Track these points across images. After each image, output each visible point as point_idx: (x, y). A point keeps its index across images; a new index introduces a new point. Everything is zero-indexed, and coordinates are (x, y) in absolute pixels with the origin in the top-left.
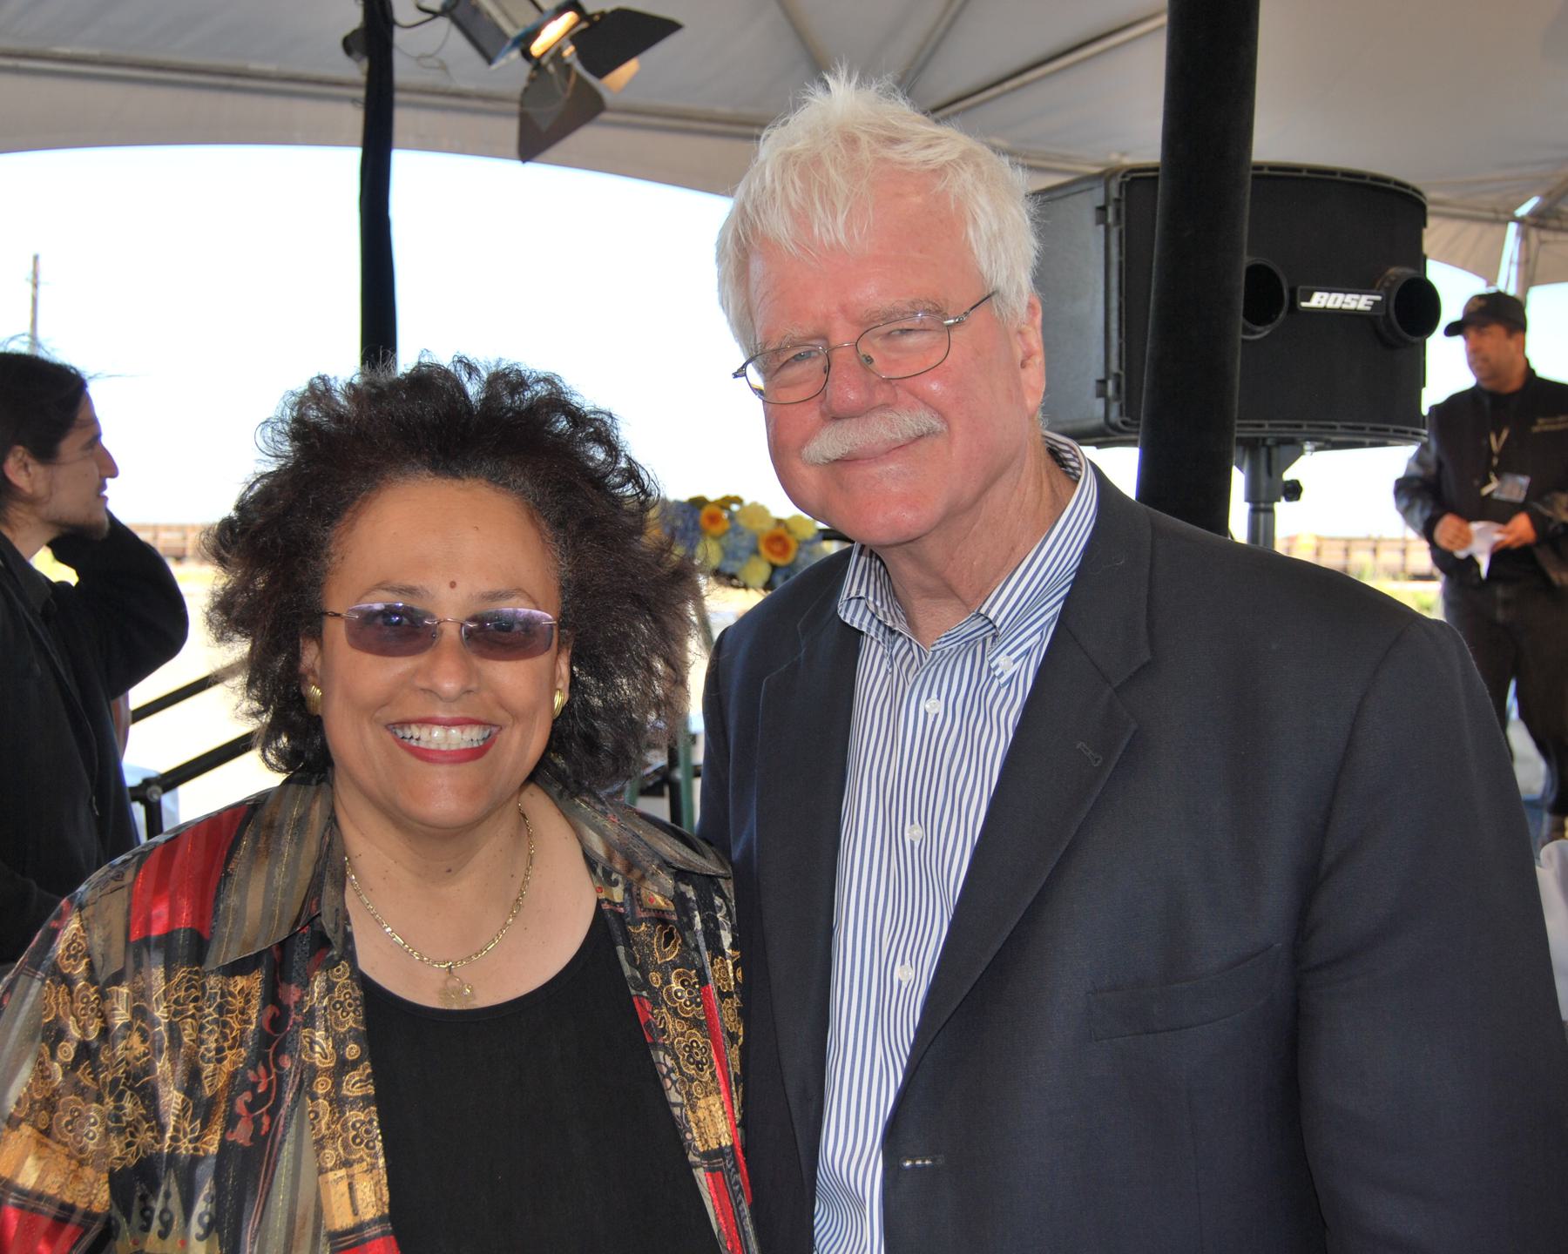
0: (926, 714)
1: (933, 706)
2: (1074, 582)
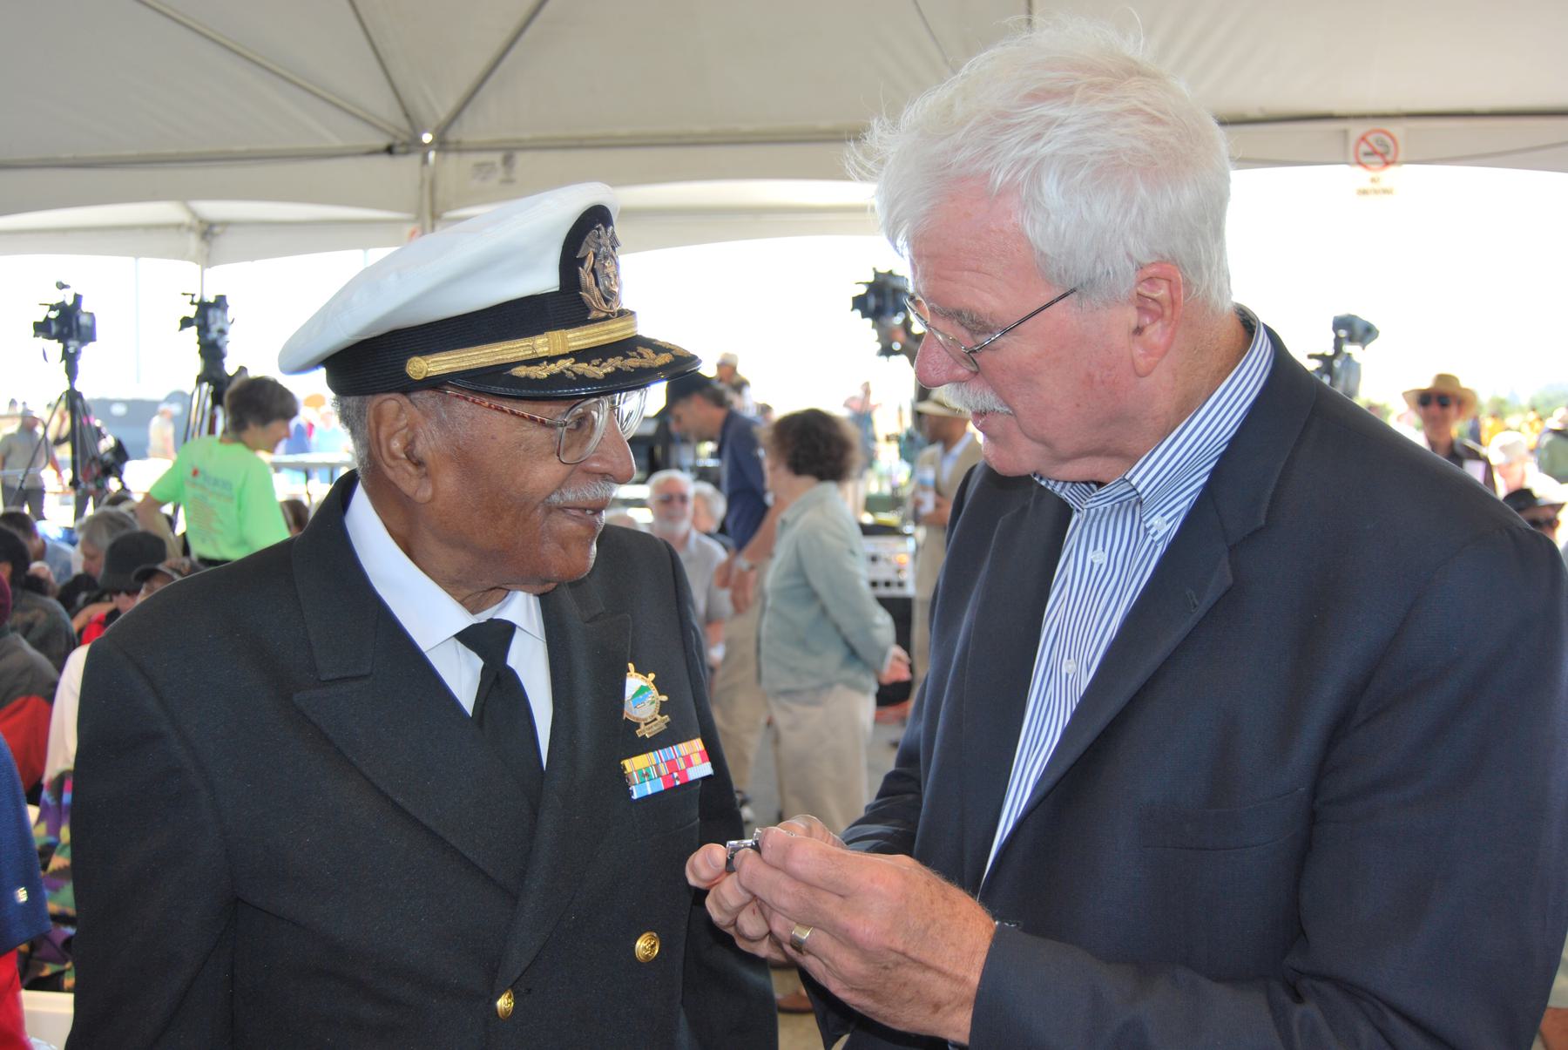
1: (1098, 557)
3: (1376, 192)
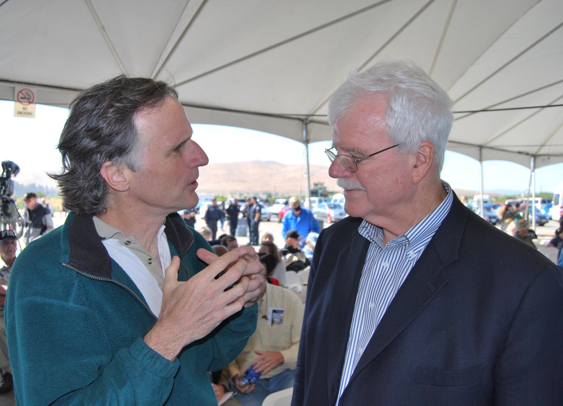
0: (383, 267)
1: (386, 264)
2: (437, 231)
3: (25, 113)
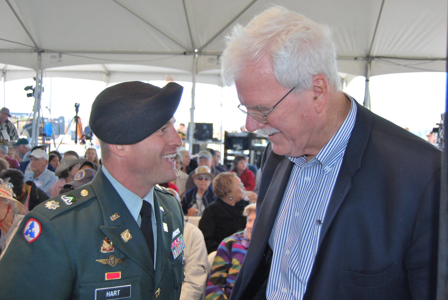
1: (308, 179)
